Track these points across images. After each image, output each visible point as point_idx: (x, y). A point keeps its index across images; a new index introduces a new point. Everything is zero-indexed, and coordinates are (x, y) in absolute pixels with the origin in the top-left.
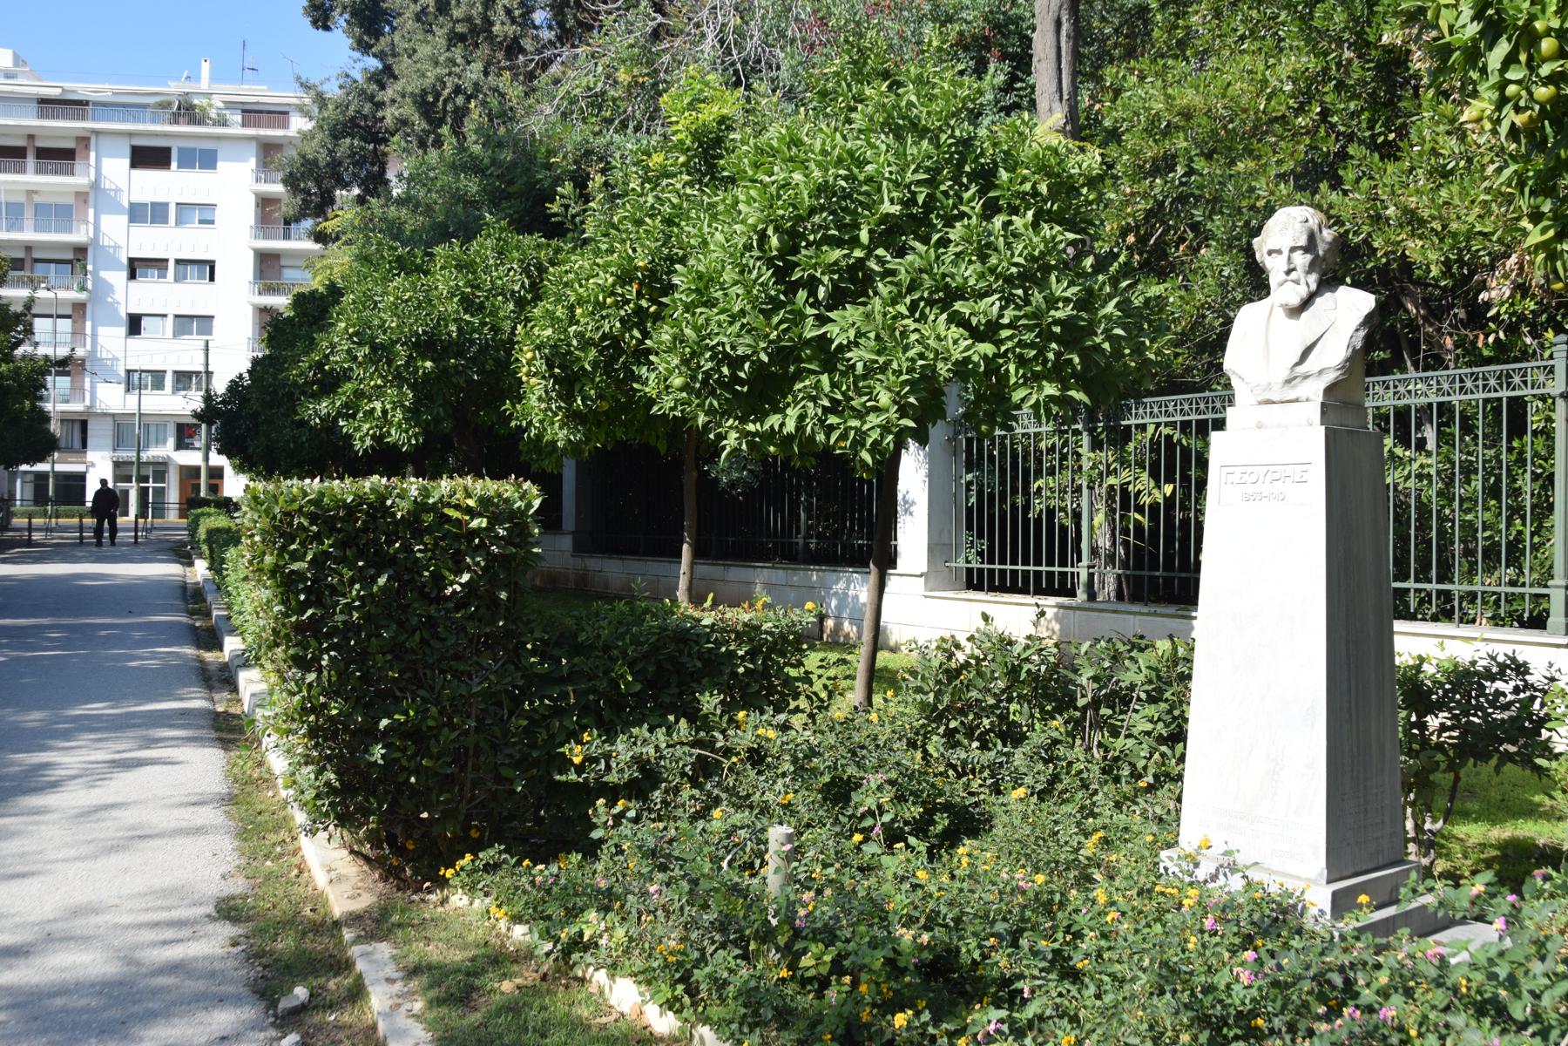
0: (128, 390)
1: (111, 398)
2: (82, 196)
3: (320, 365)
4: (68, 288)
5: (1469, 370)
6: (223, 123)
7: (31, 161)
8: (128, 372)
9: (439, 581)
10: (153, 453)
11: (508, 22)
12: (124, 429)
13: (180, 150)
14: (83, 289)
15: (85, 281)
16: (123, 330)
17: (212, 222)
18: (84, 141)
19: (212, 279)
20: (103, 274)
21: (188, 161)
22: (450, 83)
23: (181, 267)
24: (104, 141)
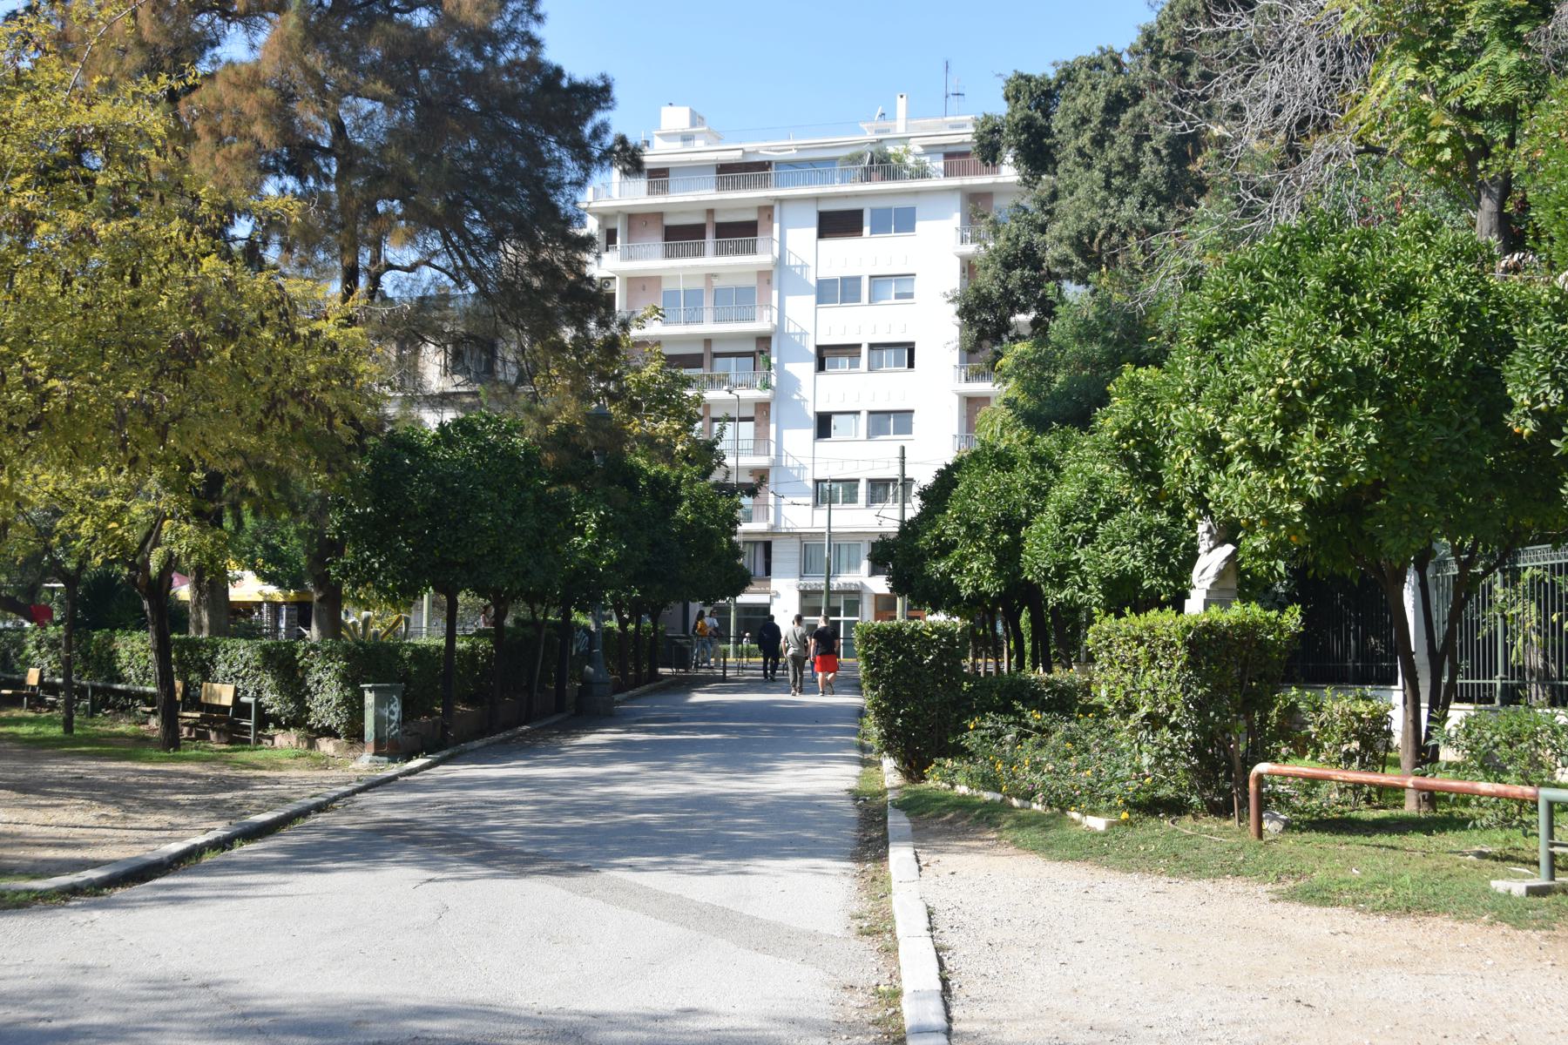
0: (816, 504)
1: (799, 515)
2: (765, 276)
3: (938, 538)
4: (750, 386)
6: (922, 173)
7: (710, 241)
8: (817, 482)
9: (922, 659)
10: (843, 580)
11: (1157, 162)
12: (816, 552)
13: (873, 210)
14: (767, 386)
15: (768, 376)
16: (810, 432)
17: (910, 296)
18: (767, 210)
19: (911, 365)
20: (789, 367)
21: (880, 227)
22: (1104, 223)
23: (875, 352)
24: (787, 207)
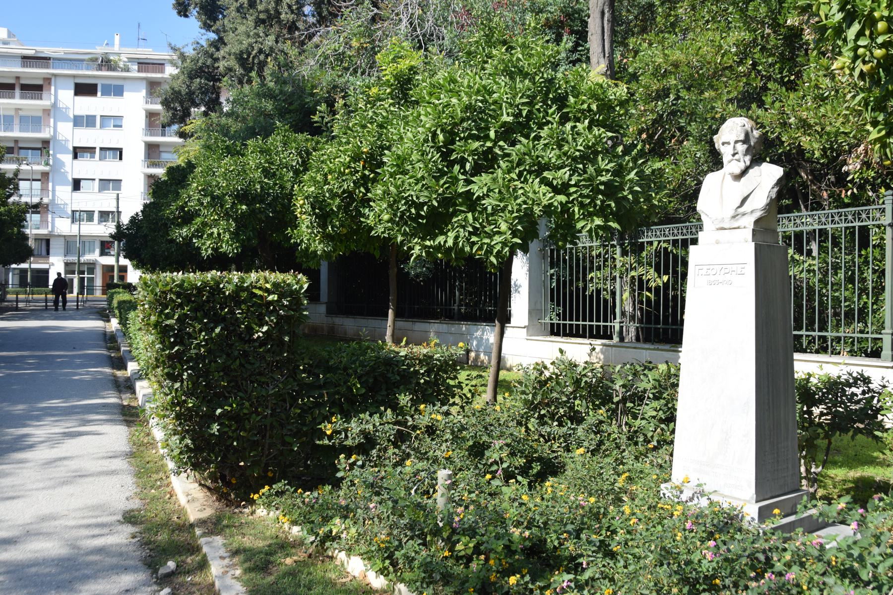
0: (73, 222)
1: (63, 226)
2: (47, 112)
3: (182, 208)
4: (38, 164)
5: (836, 211)
6: (127, 70)
7: (17, 92)
8: (73, 211)
9: (250, 330)
10: (87, 258)
11: (290, 13)
12: (70, 244)
13: (103, 85)
14: (47, 164)
15: (48, 160)
16: (70, 188)
17: (121, 126)
18: (48, 80)
19: (121, 158)
20: (59, 156)
21: (107, 92)
22: (256, 47)
23: (103, 152)
24: (59, 80)
